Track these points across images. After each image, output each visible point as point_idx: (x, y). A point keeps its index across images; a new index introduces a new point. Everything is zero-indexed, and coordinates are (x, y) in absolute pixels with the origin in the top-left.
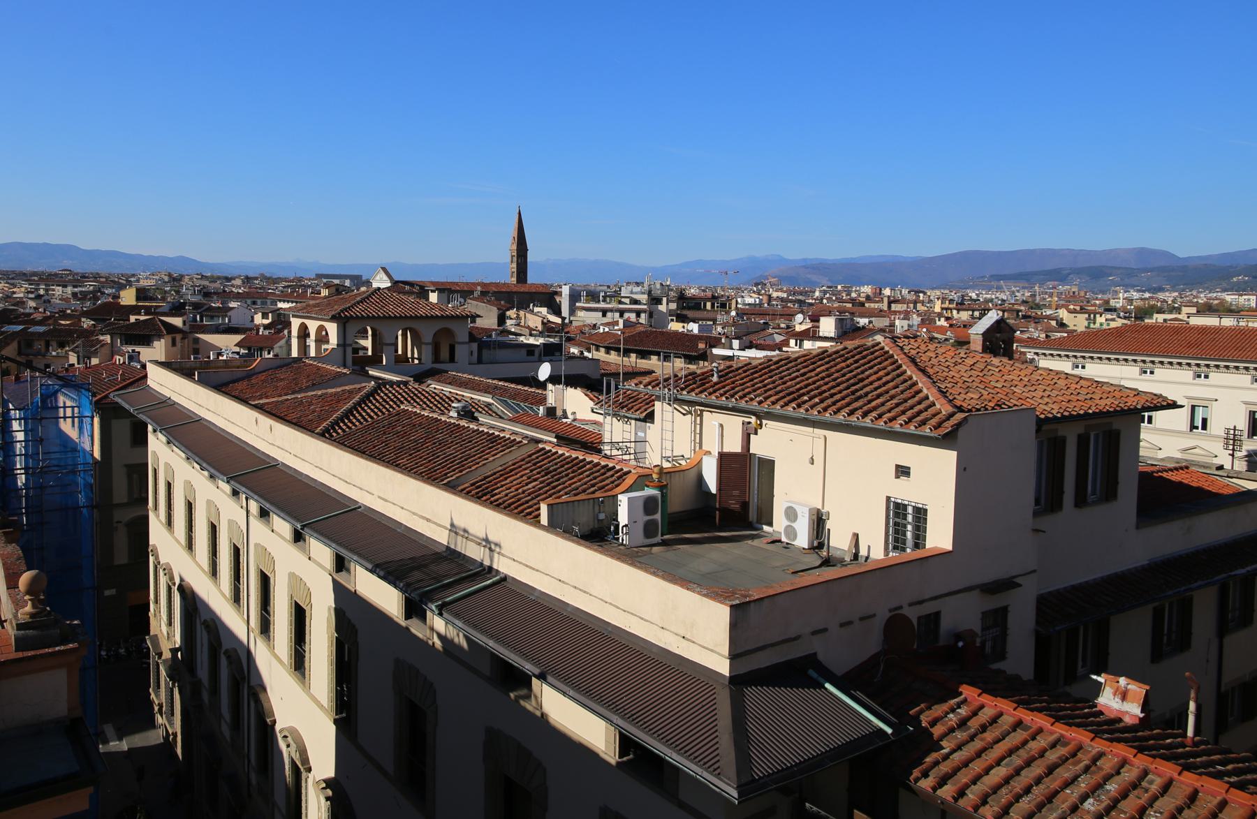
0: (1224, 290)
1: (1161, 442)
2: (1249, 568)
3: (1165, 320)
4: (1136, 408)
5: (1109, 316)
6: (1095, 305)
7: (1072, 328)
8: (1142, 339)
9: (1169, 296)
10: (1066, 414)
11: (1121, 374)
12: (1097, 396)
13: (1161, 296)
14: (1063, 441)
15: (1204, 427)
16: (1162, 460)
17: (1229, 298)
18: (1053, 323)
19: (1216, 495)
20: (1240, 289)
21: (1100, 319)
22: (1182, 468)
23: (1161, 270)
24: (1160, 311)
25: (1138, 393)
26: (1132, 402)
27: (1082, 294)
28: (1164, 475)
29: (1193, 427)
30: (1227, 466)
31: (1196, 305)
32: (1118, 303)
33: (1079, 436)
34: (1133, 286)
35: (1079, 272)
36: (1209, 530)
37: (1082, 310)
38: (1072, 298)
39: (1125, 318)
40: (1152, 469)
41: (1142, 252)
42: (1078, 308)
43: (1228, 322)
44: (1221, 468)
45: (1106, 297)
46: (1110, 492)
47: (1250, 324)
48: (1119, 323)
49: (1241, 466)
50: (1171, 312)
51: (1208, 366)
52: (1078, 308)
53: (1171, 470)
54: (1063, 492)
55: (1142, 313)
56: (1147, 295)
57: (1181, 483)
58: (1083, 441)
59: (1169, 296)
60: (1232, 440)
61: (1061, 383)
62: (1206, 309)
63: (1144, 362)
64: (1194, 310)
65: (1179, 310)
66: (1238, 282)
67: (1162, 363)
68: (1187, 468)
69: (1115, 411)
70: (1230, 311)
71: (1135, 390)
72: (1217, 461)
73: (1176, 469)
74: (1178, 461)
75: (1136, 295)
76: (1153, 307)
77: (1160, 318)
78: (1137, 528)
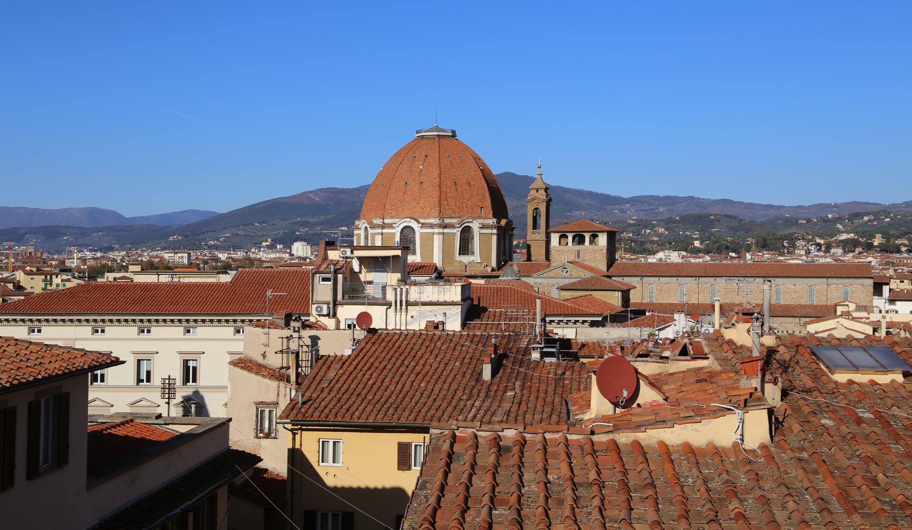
0: (163, 249)
1: (111, 399)
2: (182, 507)
3: (115, 279)
4: (83, 368)
5: (65, 277)
6: (51, 266)
7: (29, 290)
8: (97, 300)
9: (117, 255)
10: (15, 382)
11: (60, 334)
12: (46, 361)
13: (111, 255)
14: (13, 412)
15: (148, 380)
16: (111, 416)
17: (167, 256)
18: (10, 286)
19: (157, 442)
20: (175, 248)
21: (57, 280)
22: (127, 422)
23: (111, 229)
24: (111, 270)
25: (84, 353)
26: (80, 363)
27: (39, 255)
28: (113, 431)
29: (139, 381)
30: (165, 415)
31: (141, 263)
32: (73, 263)
33: (30, 404)
34: (86, 246)
35: (35, 231)
36: (153, 476)
37: (39, 272)
38: (28, 259)
39: (80, 278)
40: (102, 427)
41: (93, 212)
42: (34, 269)
43: (164, 279)
44: (159, 416)
45: (61, 257)
46: (61, 459)
47: (182, 280)
48: (75, 283)
49: (176, 412)
50: (120, 271)
51: (149, 321)
52: (34, 269)
53: (118, 425)
54: (14, 467)
55: (95, 272)
56: (99, 254)
57: (127, 436)
58: (34, 409)
59: (117, 255)
60: (168, 389)
61: (11, 350)
62: (150, 267)
63: (31, 320)
64: (138, 268)
65: (126, 269)
66: (174, 241)
67: (111, 321)
68: (132, 421)
69: (64, 374)
70: (168, 268)
71: (83, 350)
72: (158, 411)
73: (123, 424)
74: (124, 415)
75: (89, 255)
76: (104, 266)
77: (110, 276)
78: (88, 489)
